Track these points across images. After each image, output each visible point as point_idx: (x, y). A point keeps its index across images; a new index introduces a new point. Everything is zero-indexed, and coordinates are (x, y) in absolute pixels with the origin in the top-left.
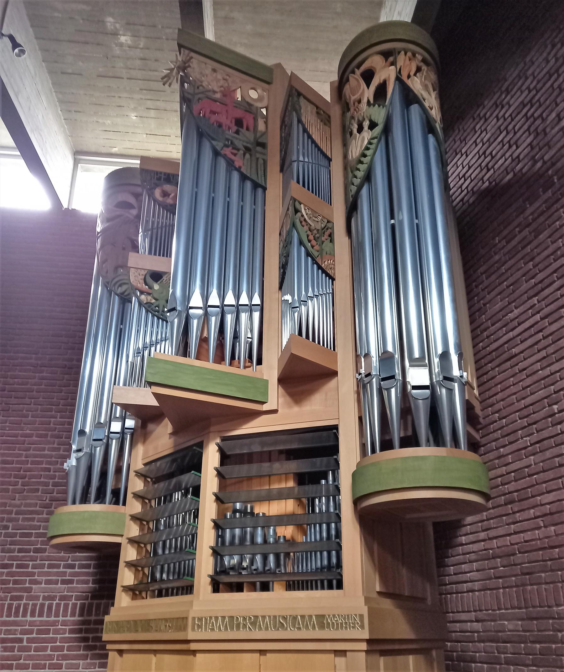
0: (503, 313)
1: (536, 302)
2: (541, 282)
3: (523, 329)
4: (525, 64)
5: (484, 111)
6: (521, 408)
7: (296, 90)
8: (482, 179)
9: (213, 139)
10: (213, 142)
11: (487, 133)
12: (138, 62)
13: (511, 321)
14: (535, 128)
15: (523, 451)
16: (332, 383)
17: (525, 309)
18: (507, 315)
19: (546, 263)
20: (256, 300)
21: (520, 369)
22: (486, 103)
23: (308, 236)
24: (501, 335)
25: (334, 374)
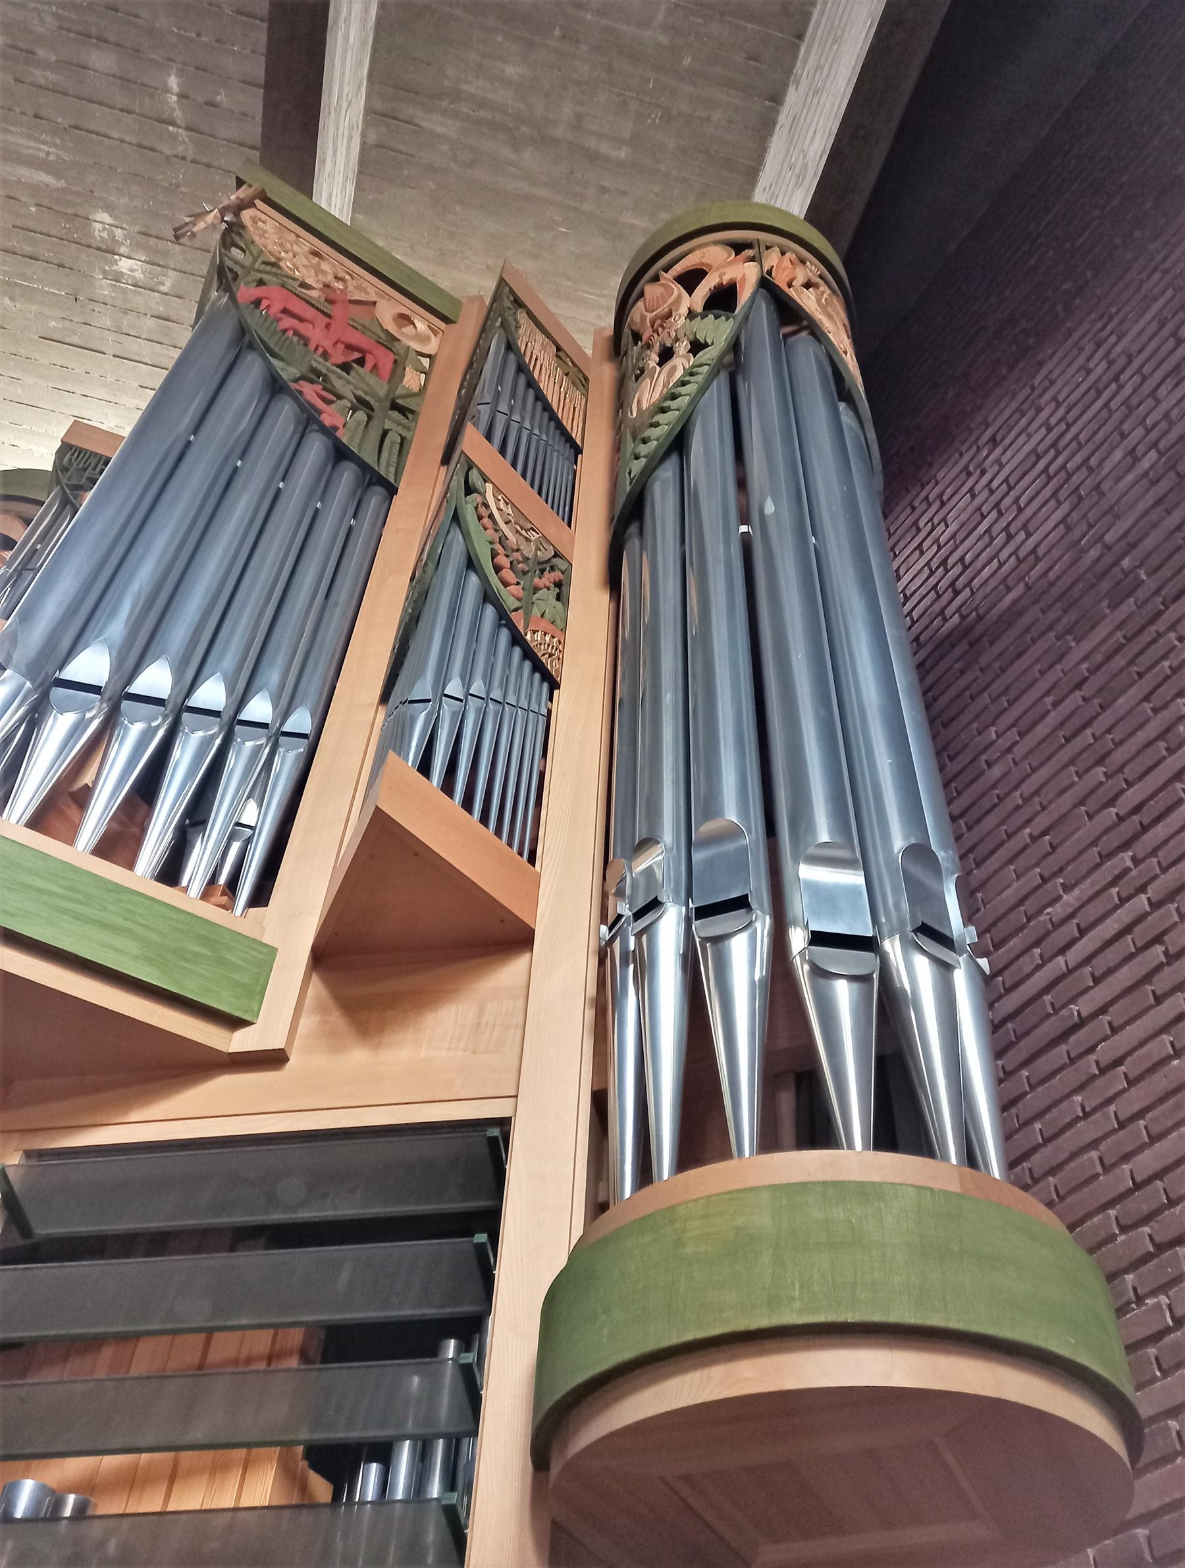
0: (1030, 906)
1: (1129, 864)
2: (1137, 809)
3: (1099, 944)
4: (1033, 389)
5: (937, 490)
6: (1121, 1189)
7: (512, 291)
8: (942, 612)
9: (274, 355)
10: (274, 361)
11: (947, 526)
12: (150, 323)
13: (1056, 926)
14: (1072, 488)
15: (1152, 1351)
16: (512, 971)
17: (1098, 887)
18: (1040, 912)
19: (1147, 759)
20: (301, 721)
21: (1104, 1063)
22: (940, 476)
23: (494, 555)
24: (1028, 969)
25: (520, 939)
